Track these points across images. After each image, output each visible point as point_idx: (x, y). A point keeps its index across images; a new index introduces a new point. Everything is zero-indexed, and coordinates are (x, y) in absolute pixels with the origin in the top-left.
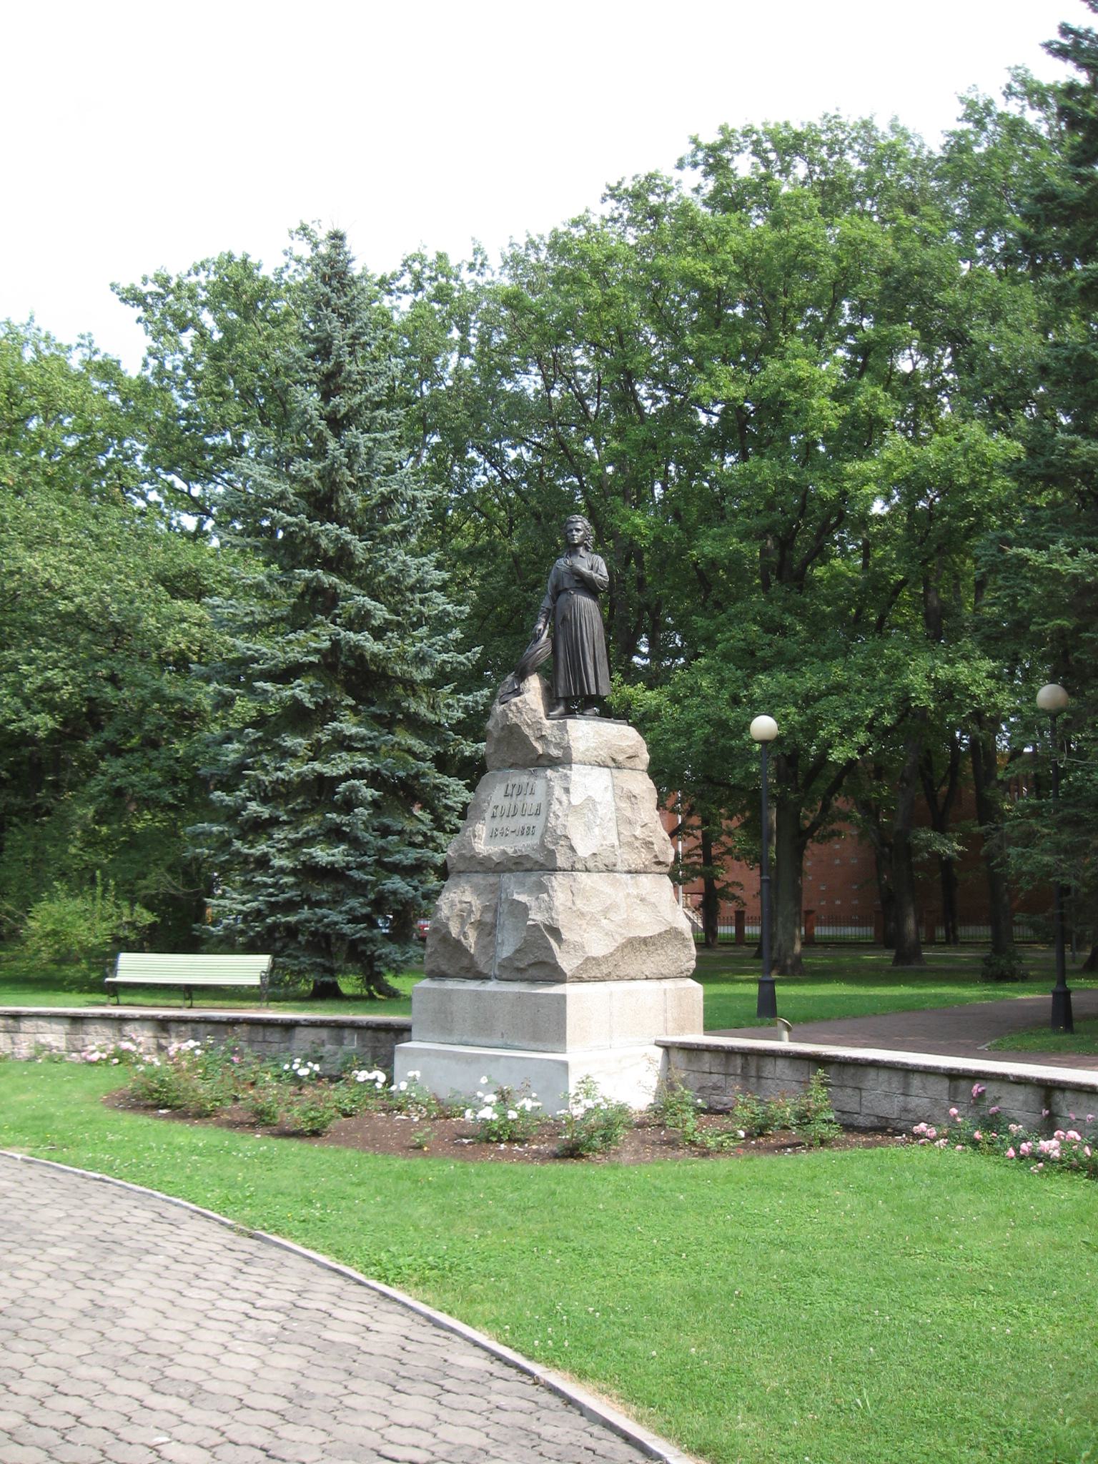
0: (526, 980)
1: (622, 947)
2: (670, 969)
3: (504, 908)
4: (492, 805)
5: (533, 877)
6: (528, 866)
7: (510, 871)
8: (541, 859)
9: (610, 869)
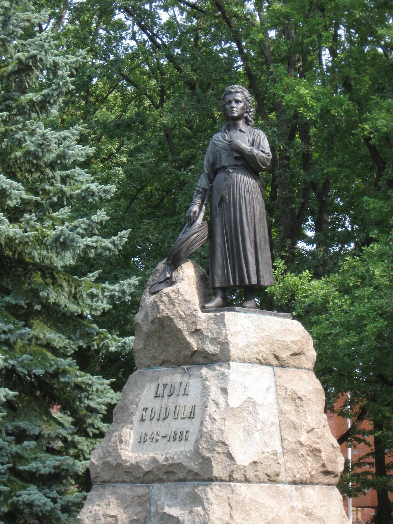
4: (141, 407)
6: (181, 475)
7: (161, 481)
9: (272, 479)
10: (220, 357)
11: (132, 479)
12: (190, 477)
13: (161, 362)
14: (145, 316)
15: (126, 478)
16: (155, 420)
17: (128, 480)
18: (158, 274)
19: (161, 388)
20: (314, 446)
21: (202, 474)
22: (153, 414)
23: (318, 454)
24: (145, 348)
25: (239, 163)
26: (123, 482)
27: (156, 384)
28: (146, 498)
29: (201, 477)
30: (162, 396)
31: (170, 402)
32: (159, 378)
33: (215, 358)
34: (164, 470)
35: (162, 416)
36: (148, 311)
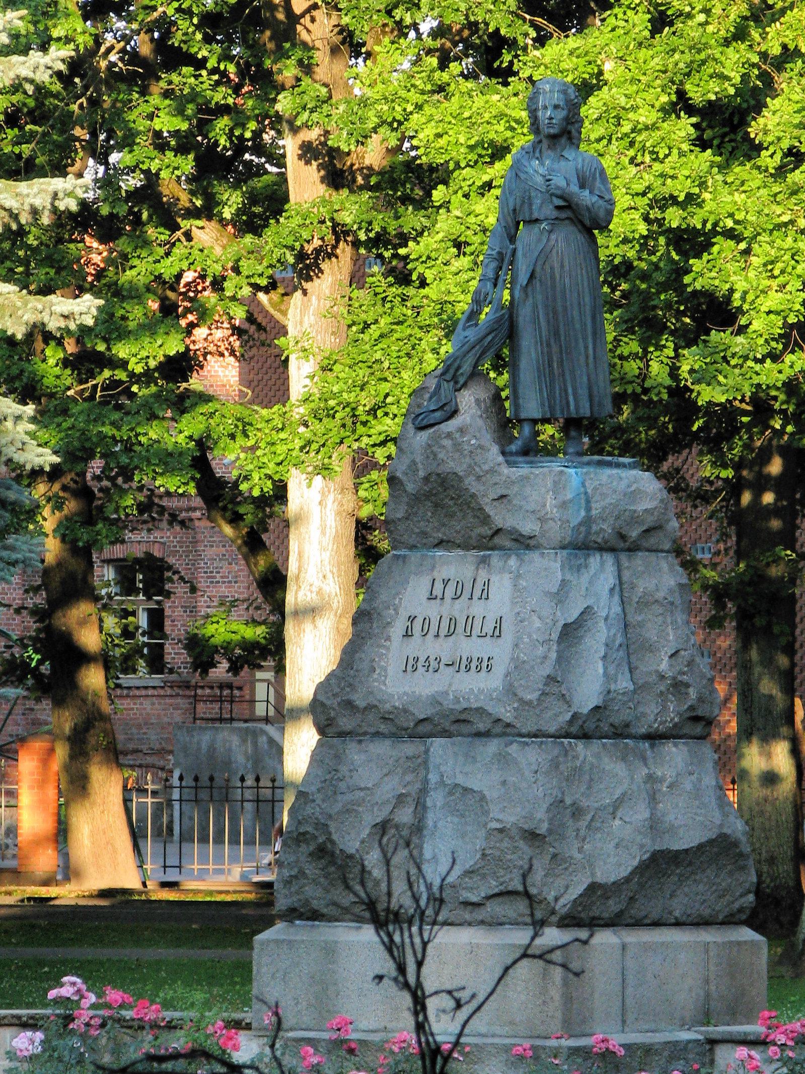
0: (482, 922)
1: (643, 869)
2: (722, 907)
3: (436, 799)
4: (404, 614)
5: (493, 746)
6: (481, 726)
7: (446, 733)
8: (507, 715)
9: (620, 733)
10: (541, 541)
11: (394, 730)
12: (498, 729)
13: (436, 541)
14: (409, 467)
15: (383, 728)
16: (430, 636)
17: (386, 731)
18: (427, 396)
19: (439, 586)
20: (680, 678)
21: (518, 725)
22: (426, 627)
23: (683, 690)
24: (407, 519)
25: (563, 215)
26: (377, 734)
27: (430, 578)
28: (419, 760)
29: (516, 731)
30: (443, 599)
31: (459, 610)
32: (433, 568)
33: (532, 542)
34: (452, 718)
35: (444, 631)
36: (418, 460)
